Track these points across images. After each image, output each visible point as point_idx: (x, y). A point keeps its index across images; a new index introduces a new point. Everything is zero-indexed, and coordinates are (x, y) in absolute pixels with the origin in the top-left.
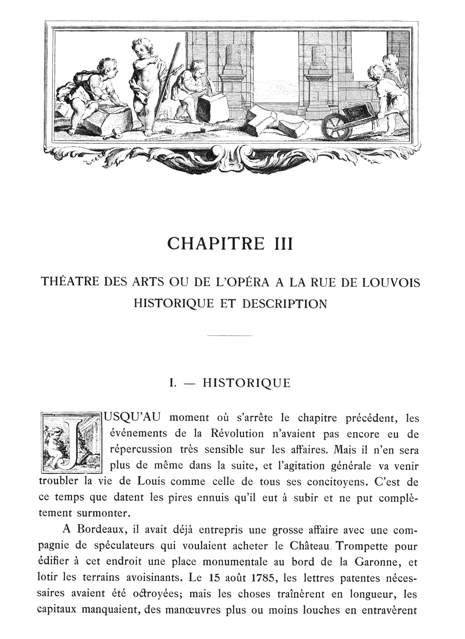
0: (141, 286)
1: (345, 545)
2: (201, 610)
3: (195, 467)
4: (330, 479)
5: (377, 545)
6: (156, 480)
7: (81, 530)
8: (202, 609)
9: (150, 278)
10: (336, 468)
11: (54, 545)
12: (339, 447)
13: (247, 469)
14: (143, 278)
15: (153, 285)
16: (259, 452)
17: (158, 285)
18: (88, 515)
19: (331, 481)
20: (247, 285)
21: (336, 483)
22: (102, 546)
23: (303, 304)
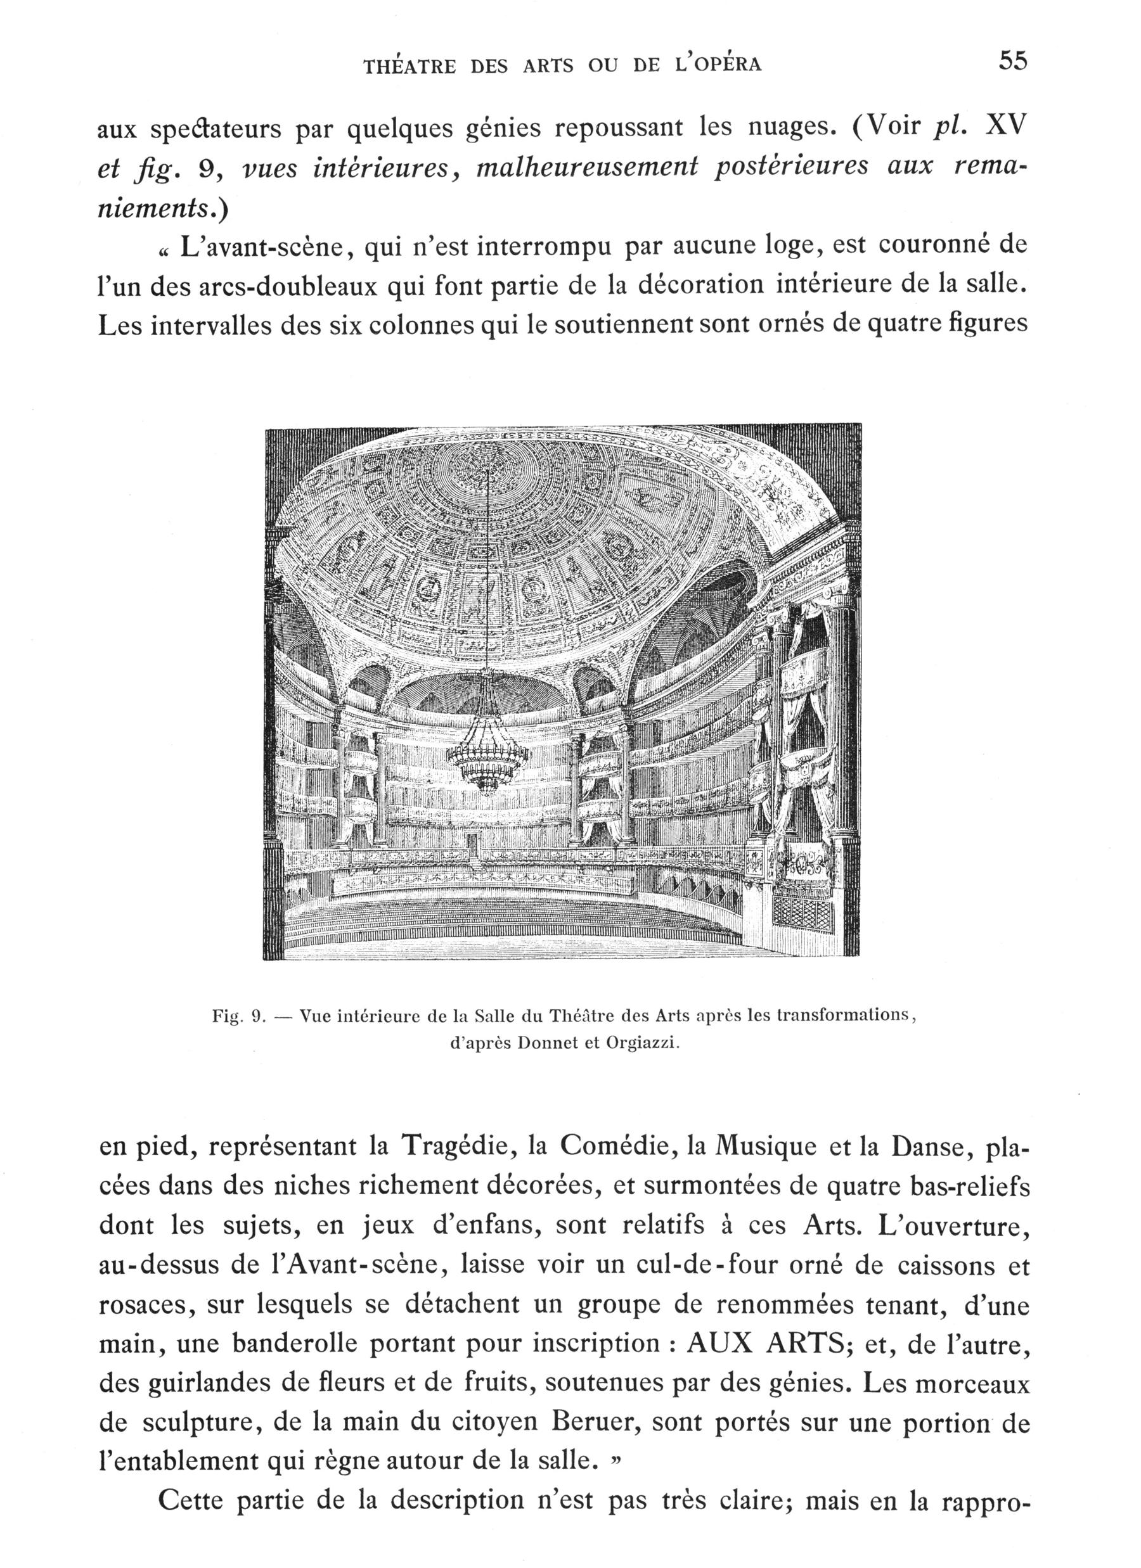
0: (788, 1354)
2: (935, 1227)
4: (465, 1415)
5: (197, 1497)
6: (293, 1458)
7: (561, 1424)
8: (938, 1224)
9: (810, 1333)
10: (781, 1388)
11: (352, 1461)
12: (727, 1139)
13: (504, 254)
14: (792, 1334)
15: (817, 1350)
16: (255, 136)
17: (831, 1350)
18: (229, 1426)
19: (468, 1419)
21: (421, 1463)
22: (170, 131)
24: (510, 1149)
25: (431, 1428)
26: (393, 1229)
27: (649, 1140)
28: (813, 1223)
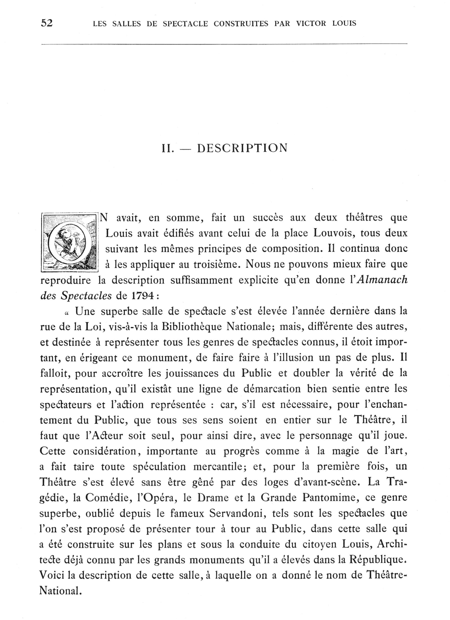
1: (396, 481)
3: (380, 313)
4: (308, 542)
20: (174, 26)
21: (314, 546)
23: (261, 148)
24: (129, 499)
25: (293, 547)
26: (196, 515)
27: (56, 495)
28: (381, 543)
